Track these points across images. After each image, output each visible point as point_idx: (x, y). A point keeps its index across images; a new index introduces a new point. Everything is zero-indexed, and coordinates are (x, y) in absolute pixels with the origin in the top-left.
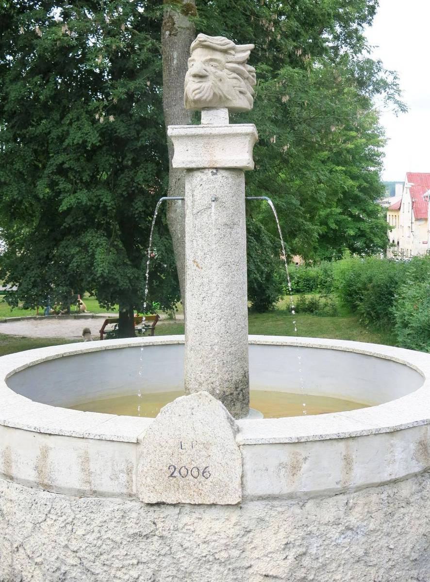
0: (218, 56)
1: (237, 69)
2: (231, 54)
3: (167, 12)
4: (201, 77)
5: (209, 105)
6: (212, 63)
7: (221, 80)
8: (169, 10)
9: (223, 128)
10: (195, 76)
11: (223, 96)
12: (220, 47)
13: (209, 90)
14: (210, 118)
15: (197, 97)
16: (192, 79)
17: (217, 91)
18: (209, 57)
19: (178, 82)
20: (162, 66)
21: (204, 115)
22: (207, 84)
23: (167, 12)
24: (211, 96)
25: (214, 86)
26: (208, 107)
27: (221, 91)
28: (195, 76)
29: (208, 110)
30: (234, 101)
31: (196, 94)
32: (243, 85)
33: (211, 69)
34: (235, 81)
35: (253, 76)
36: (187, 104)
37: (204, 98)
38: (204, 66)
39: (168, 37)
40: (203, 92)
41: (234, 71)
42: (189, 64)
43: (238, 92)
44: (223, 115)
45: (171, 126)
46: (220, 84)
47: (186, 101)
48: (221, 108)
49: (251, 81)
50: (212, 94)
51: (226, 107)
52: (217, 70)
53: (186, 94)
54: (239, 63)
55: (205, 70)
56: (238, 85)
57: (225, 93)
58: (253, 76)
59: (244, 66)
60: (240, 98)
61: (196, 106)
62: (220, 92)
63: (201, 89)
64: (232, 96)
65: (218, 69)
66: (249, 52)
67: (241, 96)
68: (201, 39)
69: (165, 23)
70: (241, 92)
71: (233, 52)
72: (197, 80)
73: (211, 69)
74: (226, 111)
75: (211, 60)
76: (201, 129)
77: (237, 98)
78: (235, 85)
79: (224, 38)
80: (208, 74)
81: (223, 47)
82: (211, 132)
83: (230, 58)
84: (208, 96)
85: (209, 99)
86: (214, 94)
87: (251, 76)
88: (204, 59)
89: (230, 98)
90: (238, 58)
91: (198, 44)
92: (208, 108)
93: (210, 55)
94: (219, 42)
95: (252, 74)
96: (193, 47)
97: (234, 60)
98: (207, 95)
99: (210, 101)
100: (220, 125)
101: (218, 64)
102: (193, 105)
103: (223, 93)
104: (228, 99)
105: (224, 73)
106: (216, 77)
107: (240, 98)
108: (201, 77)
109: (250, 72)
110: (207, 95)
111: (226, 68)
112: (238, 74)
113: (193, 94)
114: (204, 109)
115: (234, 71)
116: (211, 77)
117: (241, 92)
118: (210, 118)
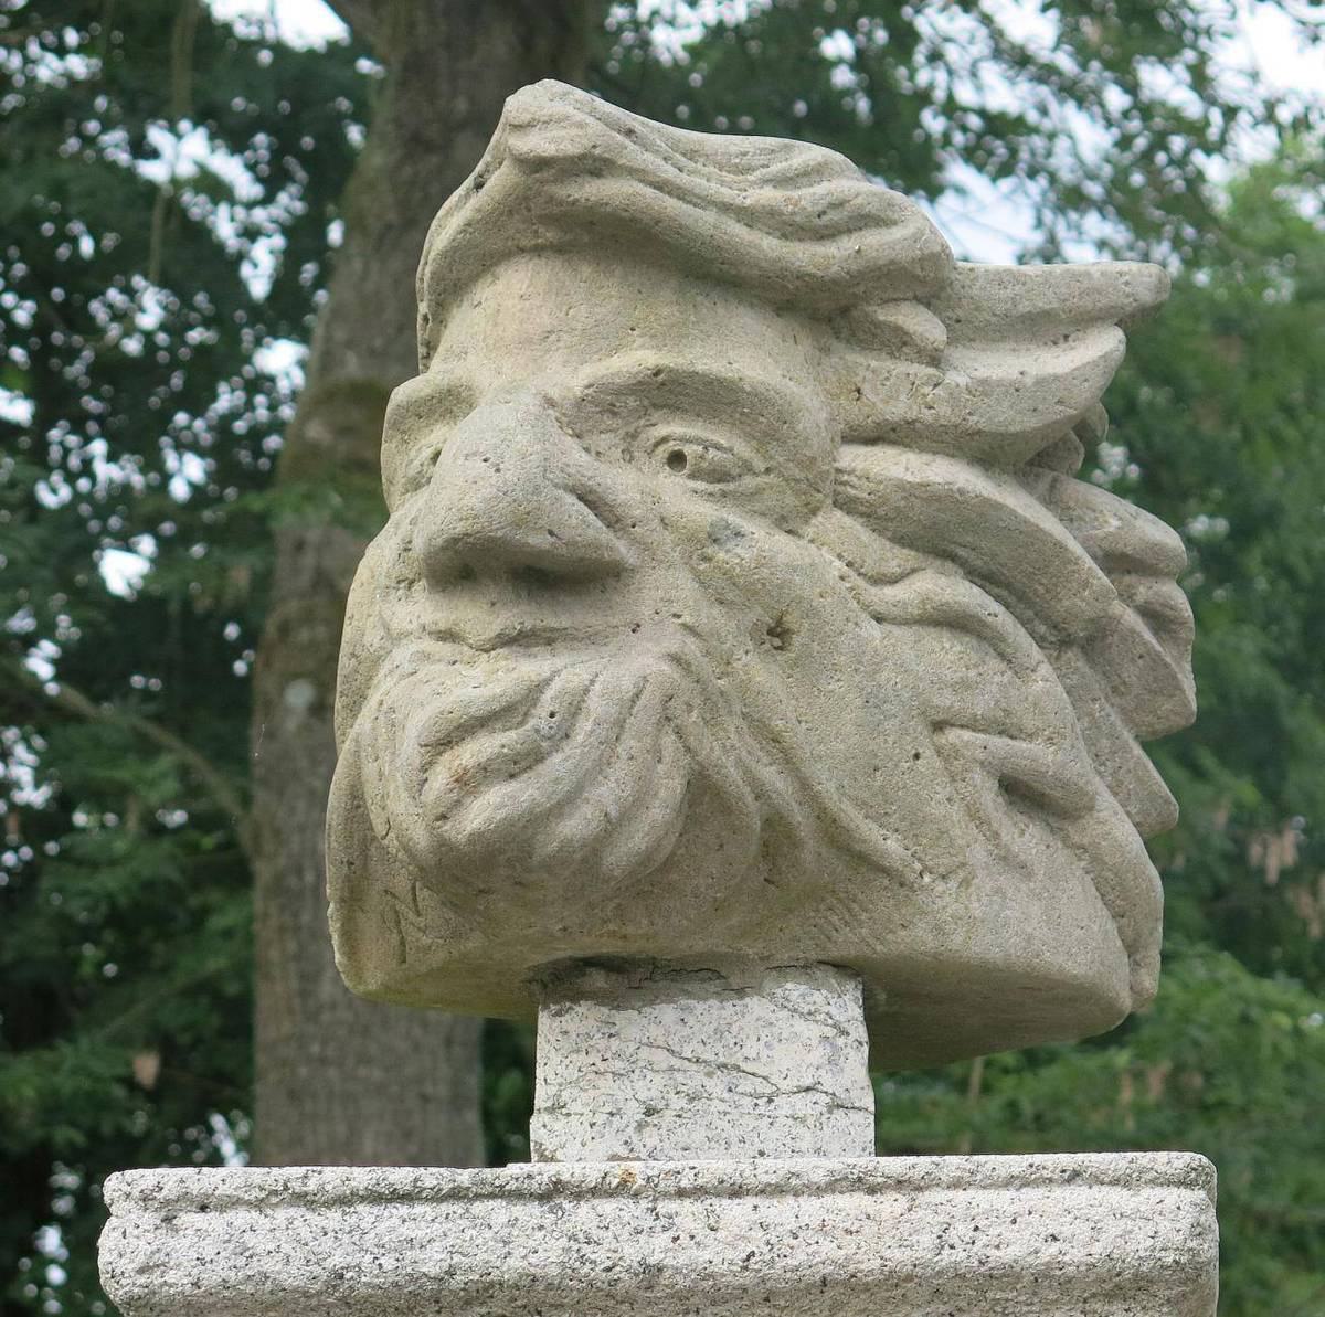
0: (748, 352)
1: (983, 515)
2: (898, 343)
3: (300, 546)
4: (527, 575)
5: (639, 935)
6: (673, 428)
7: (778, 634)
8: (313, 536)
9: (811, 1208)
10: (463, 566)
11: (799, 817)
12: (768, 246)
13: (630, 743)
14: (649, 1088)
15: (483, 812)
16: (421, 609)
17: (733, 756)
18: (637, 358)
19: (363, 1059)
20: (250, 939)
21: (561, 1049)
22: (604, 673)
23: (300, 546)
24: (659, 812)
25: (699, 694)
26: (613, 965)
27: (788, 760)
28: (463, 566)
29: (613, 1000)
30: (944, 898)
31: (468, 783)
32: (1043, 707)
33: (638, 484)
34: (948, 654)
35: (1157, 618)
36: (369, 924)
37: (575, 826)
38: (576, 457)
39: (305, 728)
40: (558, 764)
41: (932, 532)
42: (397, 458)
43: (989, 796)
44: (806, 1042)
45: (145, 1178)
46: (760, 672)
47: (353, 898)
48: (782, 970)
49: (1131, 673)
50: (670, 787)
51: (844, 968)
52: (734, 518)
53: (356, 796)
54: (988, 452)
55: (590, 499)
56: (981, 705)
57: (827, 786)
58: (1157, 618)
59: (1051, 500)
60: (1008, 860)
61: (474, 943)
62: (772, 776)
63: (539, 719)
64: (912, 824)
65: (744, 500)
66: (1107, 343)
67: (1027, 838)
68: (537, 144)
69: (285, 629)
70: (1021, 792)
71: (923, 324)
72: (479, 616)
73: (638, 484)
74: (847, 1007)
75: (665, 392)
76: (530, 1212)
77: (979, 853)
78: (945, 700)
79: (811, 153)
80: (623, 550)
81: (805, 256)
82: (656, 1248)
83: (892, 386)
84: (639, 802)
85: (635, 841)
86: (703, 792)
87: (1131, 618)
88: (573, 378)
89: (892, 847)
90: (984, 387)
91: (516, 206)
92: (625, 977)
93: (657, 340)
94: (769, 196)
95: (1145, 590)
96: (452, 254)
97: (944, 412)
98: (607, 794)
99: (653, 879)
100: (770, 1170)
101: (743, 449)
102: (431, 934)
103: (804, 785)
104: (864, 862)
105: (820, 557)
106: (730, 590)
107: (1008, 860)
108: (527, 575)
109: (1119, 562)
110: (612, 795)
111: (847, 505)
112: (985, 578)
113: (440, 779)
114: (567, 980)
115: (932, 532)
116: (667, 590)
117: (1021, 792)
118: (649, 1088)
